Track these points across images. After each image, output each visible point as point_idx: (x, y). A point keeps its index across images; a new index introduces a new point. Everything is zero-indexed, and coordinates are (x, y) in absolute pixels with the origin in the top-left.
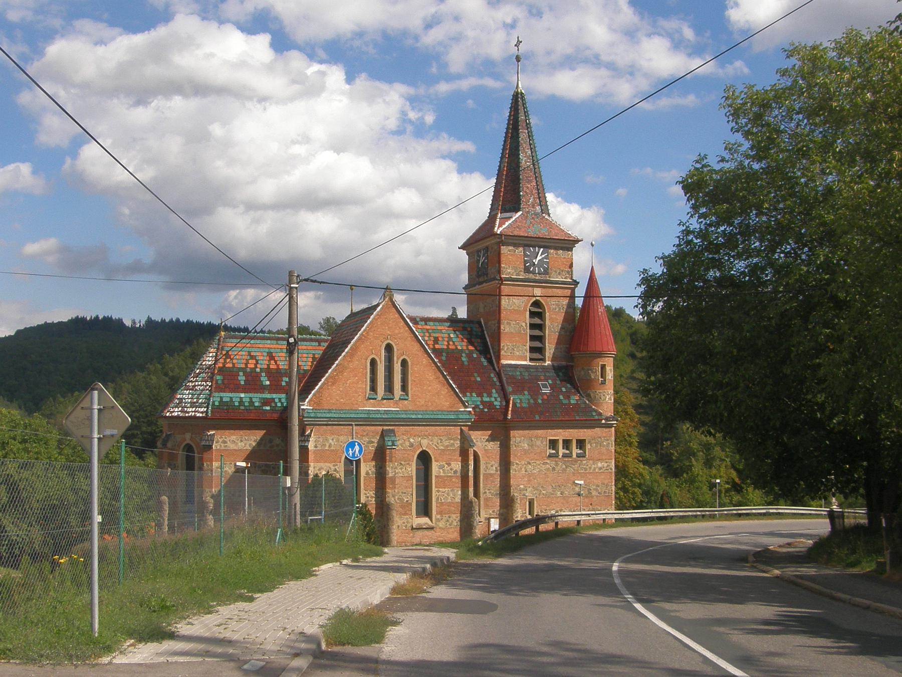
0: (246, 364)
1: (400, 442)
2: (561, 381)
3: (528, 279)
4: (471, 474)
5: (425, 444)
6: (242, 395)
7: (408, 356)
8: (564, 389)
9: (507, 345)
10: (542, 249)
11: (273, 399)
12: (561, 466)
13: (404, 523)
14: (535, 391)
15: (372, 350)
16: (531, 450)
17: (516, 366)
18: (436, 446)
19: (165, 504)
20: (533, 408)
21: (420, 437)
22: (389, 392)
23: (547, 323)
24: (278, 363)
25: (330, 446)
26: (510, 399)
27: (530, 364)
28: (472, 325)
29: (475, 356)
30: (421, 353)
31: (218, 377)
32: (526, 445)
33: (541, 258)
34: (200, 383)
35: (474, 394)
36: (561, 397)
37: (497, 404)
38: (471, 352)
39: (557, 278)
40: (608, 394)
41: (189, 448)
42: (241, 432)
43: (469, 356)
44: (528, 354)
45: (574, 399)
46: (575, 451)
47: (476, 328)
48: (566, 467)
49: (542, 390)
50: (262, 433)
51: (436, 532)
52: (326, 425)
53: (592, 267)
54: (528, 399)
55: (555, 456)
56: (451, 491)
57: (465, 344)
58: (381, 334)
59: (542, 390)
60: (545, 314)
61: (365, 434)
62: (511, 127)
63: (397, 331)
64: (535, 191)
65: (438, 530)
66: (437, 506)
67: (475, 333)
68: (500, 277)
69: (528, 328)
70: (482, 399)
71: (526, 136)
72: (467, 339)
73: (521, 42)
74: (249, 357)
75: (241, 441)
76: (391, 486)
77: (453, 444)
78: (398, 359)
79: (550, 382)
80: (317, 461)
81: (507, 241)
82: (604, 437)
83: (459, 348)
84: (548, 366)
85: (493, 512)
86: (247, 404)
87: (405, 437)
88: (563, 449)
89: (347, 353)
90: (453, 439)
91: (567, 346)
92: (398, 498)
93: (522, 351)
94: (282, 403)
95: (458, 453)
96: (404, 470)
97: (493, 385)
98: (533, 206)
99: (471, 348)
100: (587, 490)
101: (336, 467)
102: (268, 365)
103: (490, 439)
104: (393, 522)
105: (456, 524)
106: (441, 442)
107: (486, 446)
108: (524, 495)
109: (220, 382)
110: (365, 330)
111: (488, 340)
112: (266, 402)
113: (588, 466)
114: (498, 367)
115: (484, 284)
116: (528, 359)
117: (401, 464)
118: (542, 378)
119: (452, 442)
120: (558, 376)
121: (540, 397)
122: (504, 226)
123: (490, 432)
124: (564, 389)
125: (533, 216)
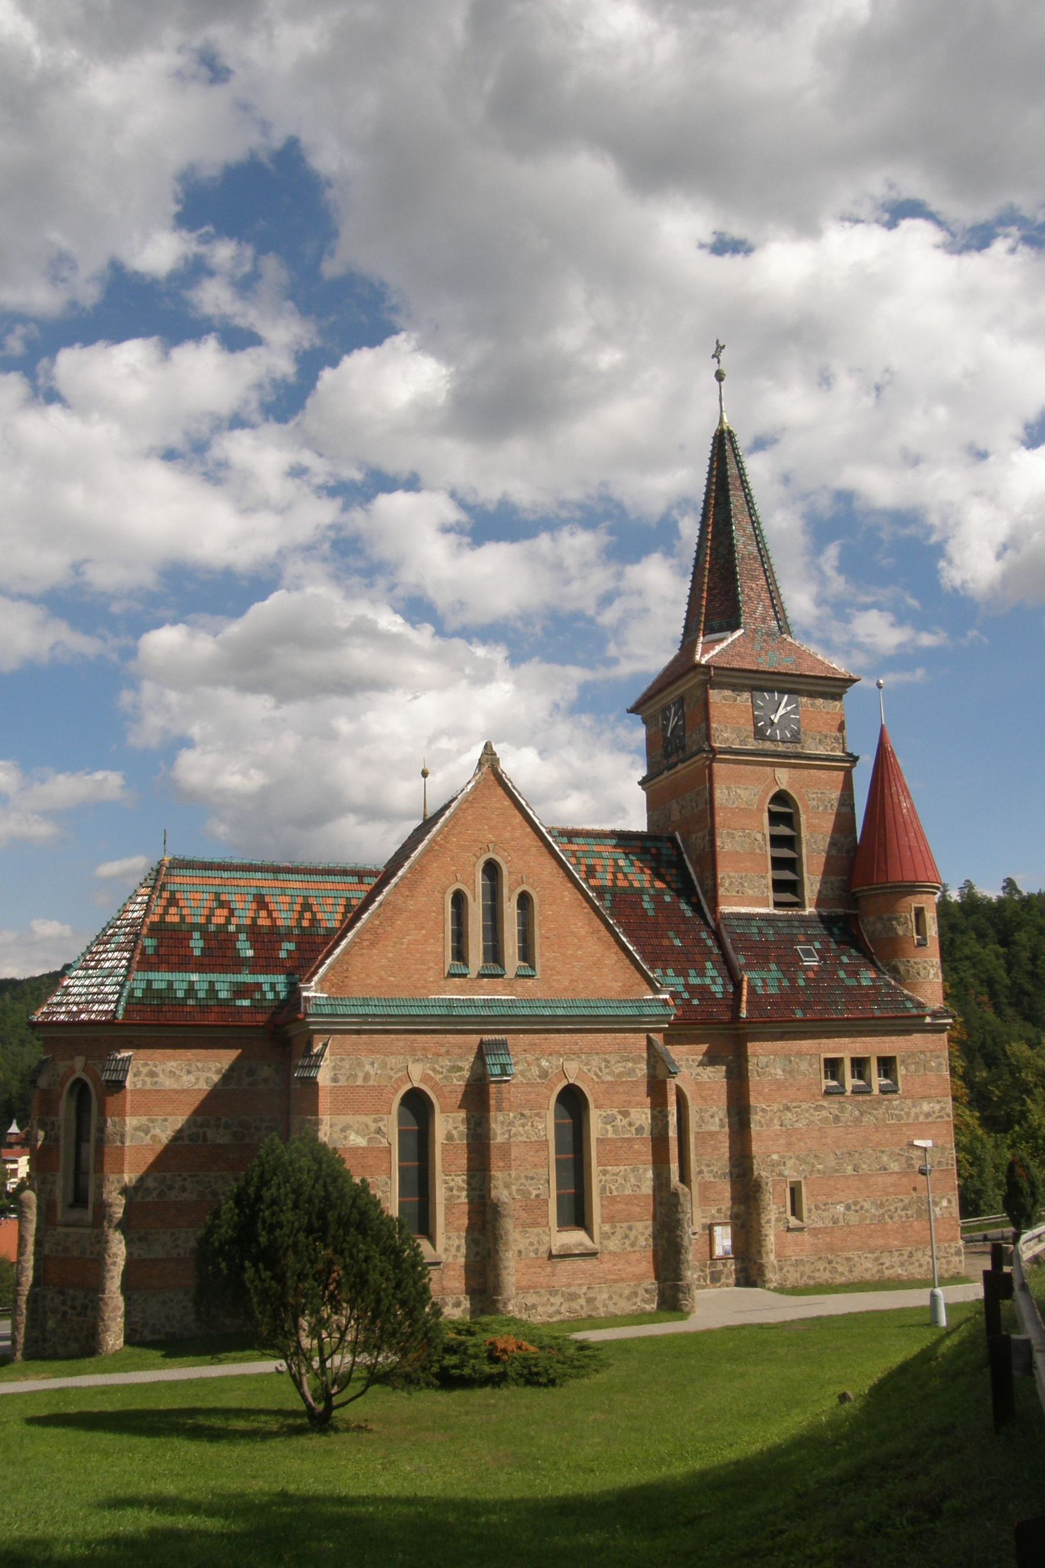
0: (209, 917)
1: (520, 1067)
2: (837, 942)
3: (763, 750)
4: (673, 1133)
5: (574, 1072)
6: (194, 977)
7: (532, 886)
8: (845, 959)
9: (730, 877)
10: (786, 697)
11: (259, 986)
12: (850, 1111)
13: (531, 1244)
14: (790, 963)
15: (455, 873)
16: (791, 1081)
17: (749, 918)
18: (596, 1074)
19: (30, 1207)
20: (787, 998)
21: (561, 1056)
22: (494, 962)
23: (804, 833)
24: (275, 915)
25: (366, 1077)
26: (742, 980)
27: (776, 912)
28: (658, 844)
29: (668, 899)
30: (560, 877)
31: (149, 942)
32: (779, 1072)
33: (784, 712)
34: (110, 955)
35: (670, 972)
36: (842, 974)
37: (717, 989)
38: (660, 893)
39: (817, 749)
40: (933, 966)
41: (80, 1090)
42: (190, 1053)
43: (657, 898)
44: (771, 894)
45: (867, 977)
46: (877, 1081)
47: (666, 850)
48: (862, 1114)
49: (803, 962)
50: (233, 1054)
51: (602, 1263)
52: (358, 1032)
53: (882, 726)
54: (779, 980)
55: (840, 1091)
56: (633, 1170)
57: (646, 877)
58: (474, 841)
59: (803, 962)
60: (799, 816)
61: (443, 1050)
62: (714, 487)
63: (507, 835)
64: (765, 595)
65: (607, 1257)
66: (602, 1206)
67: (664, 858)
68: (710, 746)
69: (768, 843)
70: (686, 980)
71: (742, 501)
72: (650, 868)
73: (724, 347)
74: (215, 904)
75: (189, 1072)
76: (501, 1164)
77: (633, 1070)
78: (511, 891)
79: (817, 945)
80: (336, 1111)
81: (719, 679)
82: (931, 1051)
83: (636, 884)
84: (810, 916)
85: (719, 1211)
86: (202, 995)
87: (530, 1057)
88: (853, 1077)
89: (402, 878)
90: (634, 1061)
91: (845, 878)
92: (518, 1190)
93: (758, 887)
94: (277, 993)
95: (643, 1089)
96: (528, 1128)
97: (707, 953)
98: (764, 620)
99: (659, 884)
100: (903, 1160)
101: (381, 1124)
102: (254, 919)
103: (706, 1059)
104: (506, 1244)
105: (644, 1243)
106: (607, 1067)
107: (698, 1074)
108: (781, 1174)
109: (150, 951)
110: (439, 832)
111: (691, 870)
112: (241, 990)
113: (902, 1110)
114: (715, 920)
115: (680, 766)
116: (771, 903)
117: (522, 1115)
118: (802, 938)
119: (630, 1065)
120: (831, 934)
121: (800, 974)
122: (713, 653)
123: (704, 1047)
124: (845, 959)
125: (765, 637)
